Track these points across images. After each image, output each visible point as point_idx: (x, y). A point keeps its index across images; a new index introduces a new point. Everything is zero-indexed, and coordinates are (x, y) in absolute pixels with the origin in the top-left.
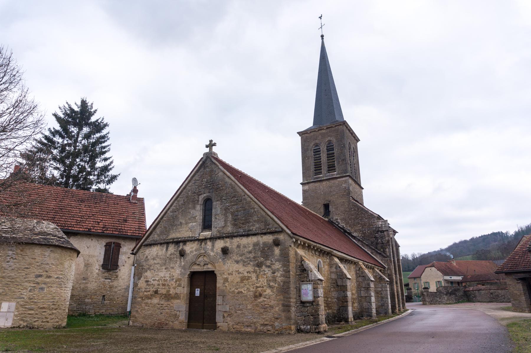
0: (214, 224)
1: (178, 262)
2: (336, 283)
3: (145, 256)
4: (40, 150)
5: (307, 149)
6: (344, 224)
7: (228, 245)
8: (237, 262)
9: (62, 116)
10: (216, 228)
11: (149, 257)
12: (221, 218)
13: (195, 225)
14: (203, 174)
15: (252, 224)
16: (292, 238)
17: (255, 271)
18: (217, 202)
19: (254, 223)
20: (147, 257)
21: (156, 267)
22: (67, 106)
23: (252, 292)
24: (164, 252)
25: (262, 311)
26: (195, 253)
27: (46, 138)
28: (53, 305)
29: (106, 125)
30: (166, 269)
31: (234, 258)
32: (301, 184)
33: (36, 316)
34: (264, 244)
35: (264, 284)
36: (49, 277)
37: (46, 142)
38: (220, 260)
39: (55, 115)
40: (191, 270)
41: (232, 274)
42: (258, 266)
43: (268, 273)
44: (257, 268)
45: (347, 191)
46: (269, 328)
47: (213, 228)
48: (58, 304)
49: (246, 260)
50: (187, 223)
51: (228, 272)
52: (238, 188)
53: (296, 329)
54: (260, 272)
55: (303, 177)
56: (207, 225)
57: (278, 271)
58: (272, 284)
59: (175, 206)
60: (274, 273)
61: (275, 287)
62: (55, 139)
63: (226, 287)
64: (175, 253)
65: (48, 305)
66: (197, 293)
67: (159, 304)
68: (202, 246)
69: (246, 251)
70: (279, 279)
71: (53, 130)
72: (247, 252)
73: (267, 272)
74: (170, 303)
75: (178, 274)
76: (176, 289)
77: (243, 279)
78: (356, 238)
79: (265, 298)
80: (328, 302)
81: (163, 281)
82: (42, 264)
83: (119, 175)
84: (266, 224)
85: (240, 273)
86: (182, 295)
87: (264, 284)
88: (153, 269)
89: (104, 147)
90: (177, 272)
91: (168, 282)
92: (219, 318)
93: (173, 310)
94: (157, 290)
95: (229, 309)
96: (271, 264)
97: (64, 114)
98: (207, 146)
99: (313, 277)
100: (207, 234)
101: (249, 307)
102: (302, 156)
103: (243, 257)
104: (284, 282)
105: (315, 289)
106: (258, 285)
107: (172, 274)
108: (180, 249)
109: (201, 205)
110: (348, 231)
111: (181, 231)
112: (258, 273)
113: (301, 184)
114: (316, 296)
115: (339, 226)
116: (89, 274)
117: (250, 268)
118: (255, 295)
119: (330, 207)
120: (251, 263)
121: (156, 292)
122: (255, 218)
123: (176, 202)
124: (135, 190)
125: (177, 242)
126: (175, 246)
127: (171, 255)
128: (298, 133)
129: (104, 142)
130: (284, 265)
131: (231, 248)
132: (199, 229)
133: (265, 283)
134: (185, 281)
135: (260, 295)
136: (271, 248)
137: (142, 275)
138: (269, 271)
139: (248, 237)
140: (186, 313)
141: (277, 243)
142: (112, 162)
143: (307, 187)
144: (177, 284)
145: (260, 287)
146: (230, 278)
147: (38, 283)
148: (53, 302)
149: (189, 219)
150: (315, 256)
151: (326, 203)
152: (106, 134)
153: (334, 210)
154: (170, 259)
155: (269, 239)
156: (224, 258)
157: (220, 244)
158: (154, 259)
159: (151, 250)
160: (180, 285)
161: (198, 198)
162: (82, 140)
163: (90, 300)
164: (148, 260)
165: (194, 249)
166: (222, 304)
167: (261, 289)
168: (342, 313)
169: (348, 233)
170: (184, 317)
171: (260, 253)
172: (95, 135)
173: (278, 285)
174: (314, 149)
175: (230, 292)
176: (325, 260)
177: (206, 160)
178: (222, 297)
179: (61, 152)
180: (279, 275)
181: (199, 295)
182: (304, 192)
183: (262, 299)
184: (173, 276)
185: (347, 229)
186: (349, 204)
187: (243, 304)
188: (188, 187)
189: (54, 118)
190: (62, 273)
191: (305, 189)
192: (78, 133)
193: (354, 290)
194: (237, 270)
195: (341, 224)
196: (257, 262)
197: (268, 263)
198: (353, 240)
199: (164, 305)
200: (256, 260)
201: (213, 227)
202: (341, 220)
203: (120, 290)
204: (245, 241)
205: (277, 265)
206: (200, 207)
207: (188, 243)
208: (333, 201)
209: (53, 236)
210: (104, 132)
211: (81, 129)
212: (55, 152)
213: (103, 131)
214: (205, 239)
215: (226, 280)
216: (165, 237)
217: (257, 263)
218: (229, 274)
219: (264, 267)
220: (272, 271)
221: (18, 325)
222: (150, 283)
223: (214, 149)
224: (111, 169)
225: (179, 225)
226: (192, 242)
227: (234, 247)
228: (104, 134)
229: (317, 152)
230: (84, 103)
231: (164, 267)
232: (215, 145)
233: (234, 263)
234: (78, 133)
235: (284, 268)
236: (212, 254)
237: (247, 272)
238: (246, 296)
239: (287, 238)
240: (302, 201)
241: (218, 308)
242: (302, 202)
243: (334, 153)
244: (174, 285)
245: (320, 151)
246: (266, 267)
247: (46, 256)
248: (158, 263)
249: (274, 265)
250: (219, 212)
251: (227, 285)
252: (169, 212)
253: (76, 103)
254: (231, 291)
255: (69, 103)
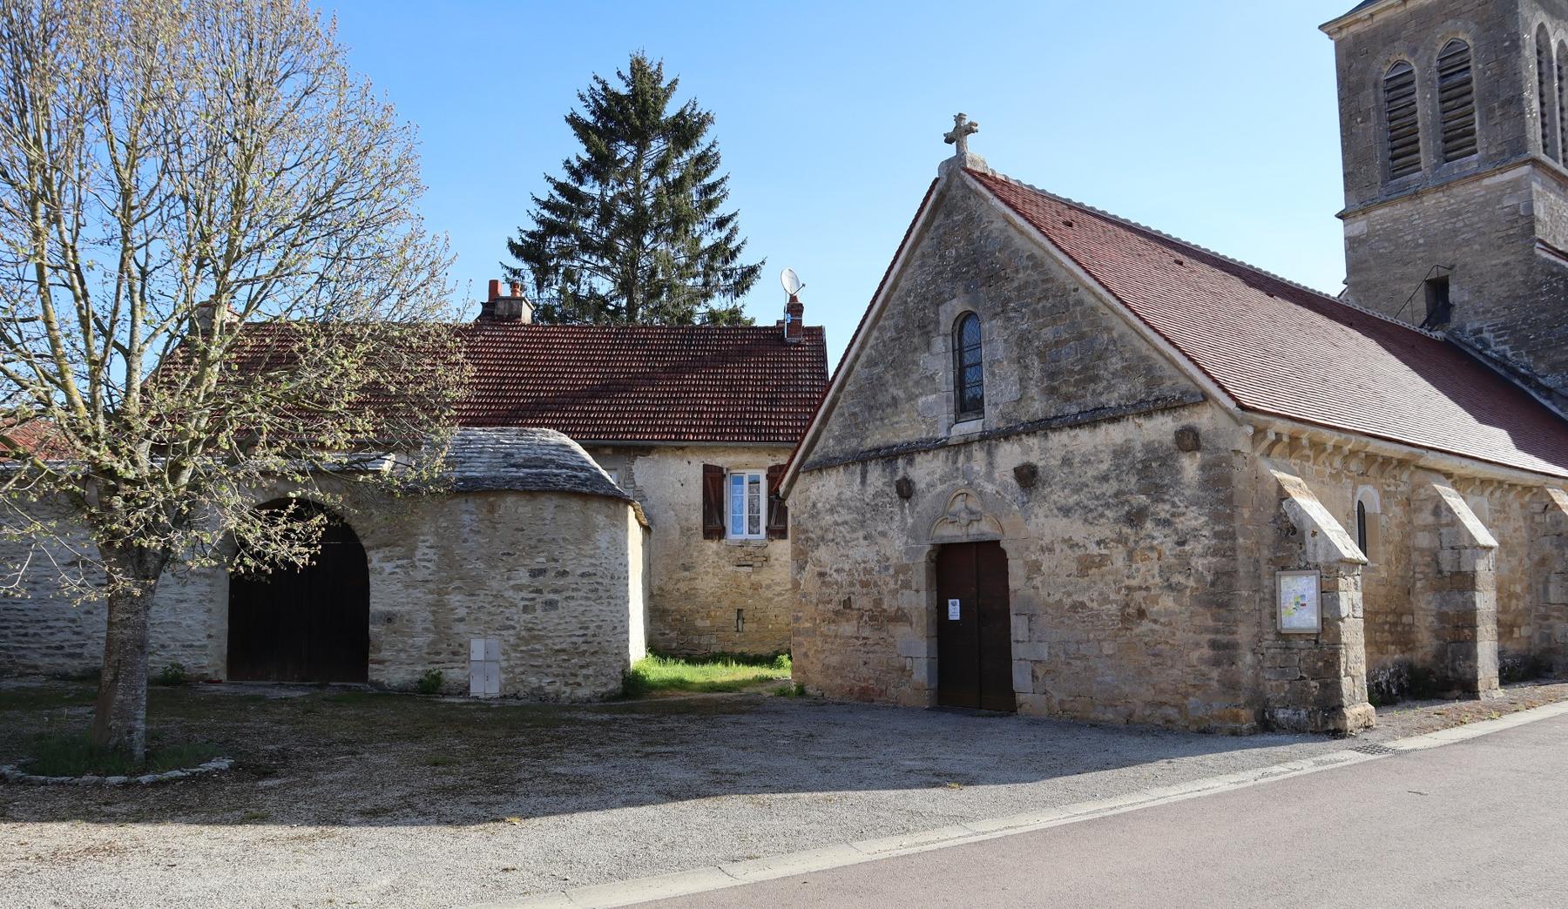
0: (989, 395)
1: (897, 518)
2: (1434, 564)
3: (810, 504)
4: (551, 228)
5: (1361, 86)
6: (1507, 347)
7: (1034, 458)
8: (1066, 511)
9: (590, 119)
10: (996, 404)
11: (819, 505)
12: (1010, 371)
13: (936, 402)
14: (945, 233)
15: (1105, 383)
16: (1239, 423)
17: (1121, 540)
18: (994, 322)
19: (1113, 382)
20: (814, 505)
21: (840, 532)
22: (598, 87)
23: (1115, 606)
24: (856, 489)
25: (1148, 661)
26: (940, 488)
27: (561, 187)
28: (586, 642)
29: (705, 121)
30: (865, 538)
31: (1055, 497)
32: (1340, 216)
33: (549, 670)
34: (1149, 448)
35: (1150, 578)
36: (564, 574)
37: (562, 200)
38: (1015, 507)
39: (574, 121)
40: (933, 542)
41: (1051, 550)
42: (1132, 520)
43: (1162, 543)
44: (1127, 530)
45: (1521, 222)
46: (1172, 712)
47: (986, 408)
48: (598, 639)
49: (1092, 504)
50: (912, 398)
51: (1040, 542)
52: (1054, 267)
53: (1259, 718)
54: (1136, 542)
55: (1345, 191)
56: (968, 404)
57: (1195, 536)
58: (1177, 578)
59: (872, 347)
60: (1181, 543)
61: (1187, 587)
62: (583, 189)
63: (1038, 588)
64: (887, 489)
65: (572, 643)
66: (954, 611)
67: (857, 638)
68: (960, 465)
69: (1089, 474)
70: (1199, 563)
71: (576, 164)
72: (1096, 478)
73: (1160, 540)
74: (884, 635)
75: (900, 552)
76: (899, 595)
77: (1087, 565)
78: (1555, 395)
79: (1155, 621)
80: (1400, 629)
81: (862, 574)
82: (539, 541)
83: (763, 263)
84: (1153, 381)
85: (1077, 544)
86: (915, 614)
87: (1150, 578)
88: (833, 540)
89: (713, 187)
90: (896, 546)
91: (876, 576)
92: (1021, 679)
93: (895, 655)
94: (849, 598)
95: (1049, 653)
96: (1173, 515)
97: (593, 113)
98: (949, 140)
99: (1320, 552)
100: (971, 427)
101: (1108, 648)
102: (1341, 115)
103: (1082, 497)
104: (1218, 574)
105: (1328, 594)
106: (1134, 583)
107: (883, 552)
108: (898, 478)
109: (946, 335)
110: (1522, 370)
111: (897, 423)
112: (1131, 544)
113: (1340, 216)
114: (1330, 620)
115: (1486, 356)
116: (695, 554)
117: (1105, 530)
118: (1123, 615)
119: (1453, 289)
120: (1108, 513)
121: (847, 604)
122: (1115, 363)
123: (875, 333)
124: (792, 306)
125: (889, 455)
126: (884, 470)
127: (875, 496)
128: (1320, 27)
129: (707, 172)
130: (1216, 517)
131: (1044, 467)
132: (945, 412)
133: (1153, 577)
134: (920, 576)
135: (1141, 614)
136: (1171, 463)
137: (806, 557)
138: (1165, 537)
139: (1095, 427)
140: (929, 665)
141: (1189, 440)
142: (734, 230)
143: (1360, 226)
144: (899, 582)
145: (1140, 588)
146: (1047, 563)
147: (539, 591)
148: (584, 635)
149: (917, 383)
150: (1348, 477)
151: (1434, 276)
152: (709, 149)
153: (1466, 298)
154: (875, 508)
155: (1162, 428)
156: (1025, 499)
157: (1010, 455)
158: (832, 511)
159: (823, 486)
160: (906, 585)
161: (937, 314)
162: (650, 178)
163: (708, 623)
164: (818, 513)
165: (937, 476)
166: (1027, 639)
167: (1144, 593)
168: (1453, 661)
169: (1524, 378)
170: (924, 674)
171: (1133, 480)
172: (681, 155)
173: (1197, 581)
174: (1388, 80)
175: (1049, 605)
176: (1392, 488)
177: (948, 186)
178: (1026, 618)
179: (604, 221)
180: (1199, 549)
181: (958, 618)
182: (1352, 244)
183: (1146, 626)
184: (888, 559)
185: (1518, 362)
186: (1530, 269)
187: (1088, 641)
188: (902, 283)
189: (569, 130)
190: (593, 561)
191: (1356, 233)
192: (637, 161)
193: (1521, 580)
194: (1067, 537)
195: (1496, 349)
196: (1126, 508)
197: (1163, 510)
198: (1542, 401)
199: (871, 642)
200: (1123, 504)
201: (986, 404)
202: (1496, 330)
203: (780, 594)
204: (1085, 440)
205: (1193, 519)
206: (945, 341)
207: (919, 459)
208: (1465, 265)
209: (559, 466)
210: (704, 141)
211: (642, 147)
212: (587, 224)
213: (701, 140)
214: (967, 443)
215: (1035, 568)
216: (854, 443)
217: (1128, 513)
218: (1042, 549)
219: (1149, 525)
220: (1175, 538)
221: (513, 691)
222: (829, 579)
223: (977, 150)
224: (738, 249)
225: (888, 405)
226: (931, 454)
227: (1055, 462)
228: (704, 149)
229: (1399, 87)
230: (638, 68)
231: (861, 534)
232: (970, 129)
233: (1057, 516)
234: (637, 161)
235: (1217, 528)
236: (989, 488)
237: (1098, 543)
238: (1098, 616)
239: (1223, 421)
240: (1345, 276)
241: (1018, 651)
242: (1345, 282)
243: (1469, 81)
244: (892, 586)
245: (1412, 82)
246: (1157, 525)
247: (548, 522)
248: (845, 523)
249: (1182, 519)
250: (1000, 354)
251: (1039, 585)
252: (858, 367)
253: (619, 73)
254: (1051, 600)
255: (601, 77)
